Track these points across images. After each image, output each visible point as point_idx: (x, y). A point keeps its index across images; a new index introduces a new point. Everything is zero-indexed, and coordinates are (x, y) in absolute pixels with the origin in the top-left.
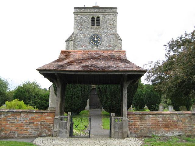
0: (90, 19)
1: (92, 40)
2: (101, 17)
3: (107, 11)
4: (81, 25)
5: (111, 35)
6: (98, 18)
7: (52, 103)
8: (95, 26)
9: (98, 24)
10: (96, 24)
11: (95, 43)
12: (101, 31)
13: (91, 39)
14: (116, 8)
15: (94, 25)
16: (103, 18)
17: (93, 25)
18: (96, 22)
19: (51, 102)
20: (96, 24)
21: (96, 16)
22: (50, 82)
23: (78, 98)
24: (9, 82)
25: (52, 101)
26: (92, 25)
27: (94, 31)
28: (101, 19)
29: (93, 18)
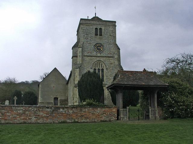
0: (94, 30)
1: (96, 48)
2: (103, 28)
3: (108, 24)
4: (87, 34)
5: (111, 44)
6: (101, 29)
7: (41, 99)
8: (98, 36)
9: (101, 35)
10: (98, 35)
11: (97, 50)
12: (103, 41)
13: (96, 47)
14: (115, 22)
15: (97, 35)
16: (104, 29)
17: (96, 35)
18: (98, 32)
19: (41, 98)
20: (98, 35)
21: (99, 27)
22: (33, 81)
23: (185, 80)
24: (37, 80)
25: (42, 97)
26: (96, 35)
27: (98, 40)
28: (103, 31)
29: (96, 29)
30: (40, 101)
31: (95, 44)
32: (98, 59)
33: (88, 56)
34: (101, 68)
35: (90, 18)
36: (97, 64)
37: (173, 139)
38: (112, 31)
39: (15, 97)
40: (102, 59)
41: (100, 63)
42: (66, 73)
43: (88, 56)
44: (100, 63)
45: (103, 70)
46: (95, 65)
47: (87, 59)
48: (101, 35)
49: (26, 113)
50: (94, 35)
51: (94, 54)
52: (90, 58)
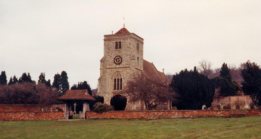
2: (122, 41)
9: (120, 48)
13: (115, 59)
26: (116, 49)
30: (239, 98)
31: (115, 57)
32: (117, 70)
33: (110, 68)
34: (120, 78)
35: (114, 33)
36: (117, 74)
37: (62, 125)
38: (130, 43)
39: (75, 103)
40: (120, 70)
41: (119, 74)
42: (221, 70)
43: (110, 68)
44: (119, 74)
45: (121, 79)
46: (115, 76)
47: (109, 71)
48: (121, 48)
49: (25, 115)
50: (114, 49)
51: (114, 65)
52: (111, 69)
